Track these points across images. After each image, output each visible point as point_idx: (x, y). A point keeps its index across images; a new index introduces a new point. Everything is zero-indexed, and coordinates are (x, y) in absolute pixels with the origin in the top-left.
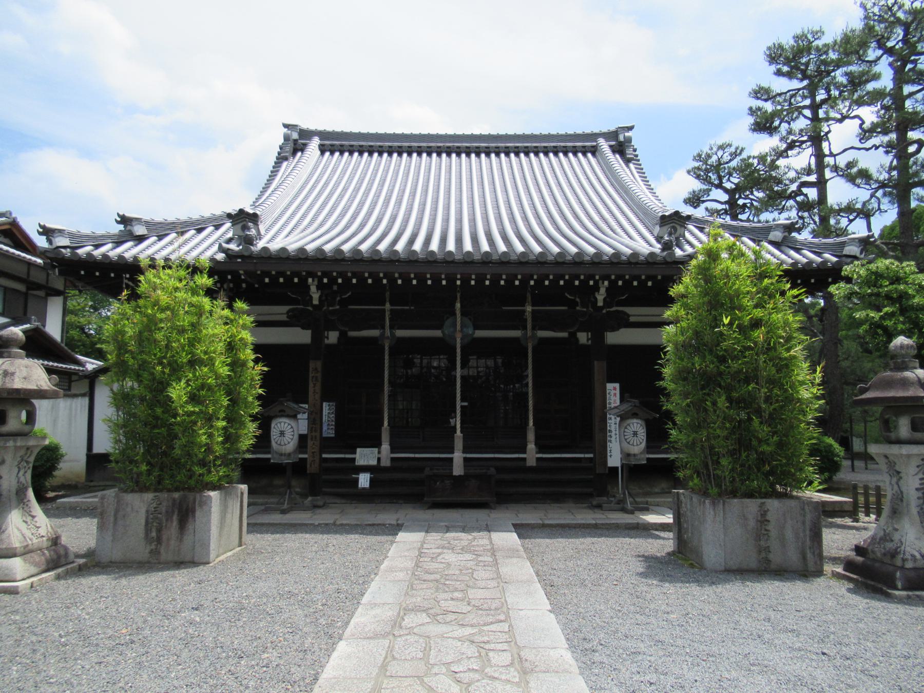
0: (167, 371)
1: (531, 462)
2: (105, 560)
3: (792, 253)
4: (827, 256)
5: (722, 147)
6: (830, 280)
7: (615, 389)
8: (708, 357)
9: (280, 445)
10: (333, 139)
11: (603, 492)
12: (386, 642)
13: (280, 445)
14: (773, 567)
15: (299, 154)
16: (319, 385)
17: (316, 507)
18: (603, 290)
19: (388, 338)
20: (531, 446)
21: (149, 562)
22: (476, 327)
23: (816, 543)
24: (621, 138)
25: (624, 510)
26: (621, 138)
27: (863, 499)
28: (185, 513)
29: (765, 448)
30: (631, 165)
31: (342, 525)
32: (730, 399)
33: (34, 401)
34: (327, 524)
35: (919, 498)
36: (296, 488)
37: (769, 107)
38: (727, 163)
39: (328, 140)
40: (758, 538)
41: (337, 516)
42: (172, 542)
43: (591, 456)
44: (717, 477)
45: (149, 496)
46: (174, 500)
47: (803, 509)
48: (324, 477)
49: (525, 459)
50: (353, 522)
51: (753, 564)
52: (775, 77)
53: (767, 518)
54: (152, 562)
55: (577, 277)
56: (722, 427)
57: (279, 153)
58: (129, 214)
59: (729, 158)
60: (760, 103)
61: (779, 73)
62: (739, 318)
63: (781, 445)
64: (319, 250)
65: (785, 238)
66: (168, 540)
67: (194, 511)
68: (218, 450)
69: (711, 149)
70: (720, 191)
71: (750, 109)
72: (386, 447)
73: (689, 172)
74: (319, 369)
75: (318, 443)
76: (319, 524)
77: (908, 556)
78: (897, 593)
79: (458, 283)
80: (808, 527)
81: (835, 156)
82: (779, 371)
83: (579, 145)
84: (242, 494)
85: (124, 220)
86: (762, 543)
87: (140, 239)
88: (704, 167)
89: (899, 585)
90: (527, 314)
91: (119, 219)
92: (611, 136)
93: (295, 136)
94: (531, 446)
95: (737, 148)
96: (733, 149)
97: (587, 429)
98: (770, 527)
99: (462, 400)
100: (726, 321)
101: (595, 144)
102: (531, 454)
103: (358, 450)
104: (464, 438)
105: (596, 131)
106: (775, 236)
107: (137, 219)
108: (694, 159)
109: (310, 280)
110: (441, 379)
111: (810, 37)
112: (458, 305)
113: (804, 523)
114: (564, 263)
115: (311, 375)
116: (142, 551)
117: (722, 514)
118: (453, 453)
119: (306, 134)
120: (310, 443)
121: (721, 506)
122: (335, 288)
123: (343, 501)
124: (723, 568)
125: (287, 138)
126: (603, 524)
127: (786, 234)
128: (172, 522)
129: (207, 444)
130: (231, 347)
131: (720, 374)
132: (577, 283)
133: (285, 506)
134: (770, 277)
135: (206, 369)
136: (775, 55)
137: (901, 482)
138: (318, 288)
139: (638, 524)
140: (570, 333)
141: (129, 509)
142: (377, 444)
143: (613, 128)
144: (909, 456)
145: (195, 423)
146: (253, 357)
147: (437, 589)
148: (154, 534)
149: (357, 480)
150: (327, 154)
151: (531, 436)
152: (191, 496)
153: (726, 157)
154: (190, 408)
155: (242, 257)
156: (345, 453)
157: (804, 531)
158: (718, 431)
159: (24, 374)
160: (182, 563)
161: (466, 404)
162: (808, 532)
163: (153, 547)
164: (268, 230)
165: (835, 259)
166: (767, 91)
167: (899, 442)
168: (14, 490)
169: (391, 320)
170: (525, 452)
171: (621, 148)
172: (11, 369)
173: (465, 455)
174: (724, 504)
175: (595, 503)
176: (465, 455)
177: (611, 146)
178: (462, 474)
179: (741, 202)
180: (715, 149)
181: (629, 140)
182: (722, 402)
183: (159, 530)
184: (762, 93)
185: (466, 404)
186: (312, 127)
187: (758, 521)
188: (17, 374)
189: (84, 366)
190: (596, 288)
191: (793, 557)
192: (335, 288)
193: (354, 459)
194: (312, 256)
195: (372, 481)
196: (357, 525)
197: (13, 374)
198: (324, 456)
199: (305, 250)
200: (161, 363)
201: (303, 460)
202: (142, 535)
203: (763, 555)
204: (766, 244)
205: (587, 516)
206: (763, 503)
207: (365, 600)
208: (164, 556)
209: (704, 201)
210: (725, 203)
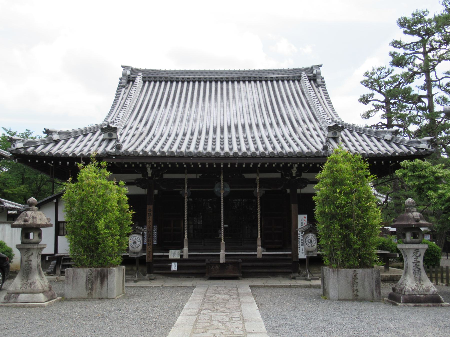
0: (95, 215)
2: (69, 297)
3: (394, 145)
4: (412, 148)
5: (379, 69)
7: (305, 218)
8: (332, 206)
9: (134, 248)
10: (150, 74)
11: (296, 271)
12: (196, 316)
13: (134, 248)
14: (359, 298)
15: (131, 83)
17: (151, 279)
18: (295, 169)
19: (187, 193)
20: (259, 248)
21: (88, 298)
24: (315, 72)
25: (306, 280)
26: (315, 72)
28: (103, 277)
29: (356, 246)
30: (320, 88)
31: (166, 287)
32: (342, 226)
33: (41, 228)
34: (158, 286)
36: (146, 267)
37: (401, 52)
38: (384, 78)
39: (148, 75)
40: (353, 285)
41: (163, 283)
43: (291, 253)
44: (336, 260)
45: (87, 269)
46: (98, 271)
47: (373, 273)
48: (154, 265)
49: (256, 255)
50: (172, 285)
51: (351, 297)
52: (404, 34)
53: (357, 277)
54: (90, 297)
56: (338, 237)
57: (120, 83)
58: (51, 128)
59: (385, 75)
60: (396, 50)
61: (405, 32)
62: (345, 189)
63: (364, 245)
65: (393, 138)
66: (96, 288)
67: (107, 276)
68: (116, 249)
69: (374, 70)
70: (380, 95)
71: (390, 53)
72: (186, 249)
73: (362, 83)
74: (152, 209)
75: (151, 247)
76: (155, 286)
77: (407, 290)
78: (400, 304)
79: (222, 166)
80: (374, 281)
81: (439, 80)
82: (363, 212)
83: (290, 77)
84: (124, 269)
85: (48, 132)
87: (57, 142)
88: (370, 81)
89: (402, 301)
90: (257, 180)
91: (45, 131)
92: (311, 69)
93: (129, 73)
94: (259, 248)
95: (389, 70)
96: (387, 70)
97: (287, 239)
98: (358, 281)
99: (225, 224)
100: (338, 191)
101: (299, 75)
102: (260, 252)
103: (170, 251)
104: (225, 244)
105: (301, 67)
106: (388, 137)
107: (55, 131)
108: (364, 75)
109: (148, 165)
111: (422, 14)
113: (373, 279)
114: (274, 157)
115: (147, 213)
116: (84, 293)
118: (220, 252)
119: (135, 71)
120: (148, 247)
121: (337, 272)
125: (124, 75)
126: (294, 286)
127: (394, 136)
128: (97, 280)
129: (112, 246)
130: (119, 202)
131: (338, 214)
133: (136, 279)
134: (362, 169)
135: (112, 214)
136: (403, 23)
137: (408, 260)
138: (151, 169)
139: (311, 285)
140: (300, 175)
141: (79, 275)
142: (181, 247)
143: (310, 66)
144: (409, 249)
145: (107, 237)
146: (129, 207)
147: (214, 305)
148: (90, 286)
150: (147, 83)
151: (259, 243)
152: (105, 269)
153: (383, 74)
154: (106, 231)
155: (116, 155)
156: (164, 253)
157: (373, 282)
158: (336, 239)
159: (40, 218)
160: (102, 298)
161: (227, 226)
162: (374, 283)
163: (90, 292)
164: (121, 134)
165: (415, 150)
166: (399, 43)
167: (407, 243)
168: (36, 266)
169: (188, 184)
170: (256, 251)
171: (314, 77)
172: (35, 216)
173: (226, 253)
174: (338, 271)
175: (292, 276)
176: (226, 253)
177: (308, 77)
178: (225, 262)
179: (392, 101)
180: (376, 70)
181: (319, 74)
182: (337, 226)
183: (92, 284)
184: (397, 44)
185: (227, 226)
186: (138, 67)
188: (38, 218)
189: (3, 204)
190: (292, 167)
193: (168, 256)
195: (178, 267)
196: (174, 287)
197: (36, 218)
198: (154, 254)
200: (92, 211)
201: (145, 256)
202: (85, 286)
203: (355, 293)
204: (382, 141)
205: (287, 282)
207: (185, 307)
208: (94, 296)
209: (370, 101)
210: (383, 102)
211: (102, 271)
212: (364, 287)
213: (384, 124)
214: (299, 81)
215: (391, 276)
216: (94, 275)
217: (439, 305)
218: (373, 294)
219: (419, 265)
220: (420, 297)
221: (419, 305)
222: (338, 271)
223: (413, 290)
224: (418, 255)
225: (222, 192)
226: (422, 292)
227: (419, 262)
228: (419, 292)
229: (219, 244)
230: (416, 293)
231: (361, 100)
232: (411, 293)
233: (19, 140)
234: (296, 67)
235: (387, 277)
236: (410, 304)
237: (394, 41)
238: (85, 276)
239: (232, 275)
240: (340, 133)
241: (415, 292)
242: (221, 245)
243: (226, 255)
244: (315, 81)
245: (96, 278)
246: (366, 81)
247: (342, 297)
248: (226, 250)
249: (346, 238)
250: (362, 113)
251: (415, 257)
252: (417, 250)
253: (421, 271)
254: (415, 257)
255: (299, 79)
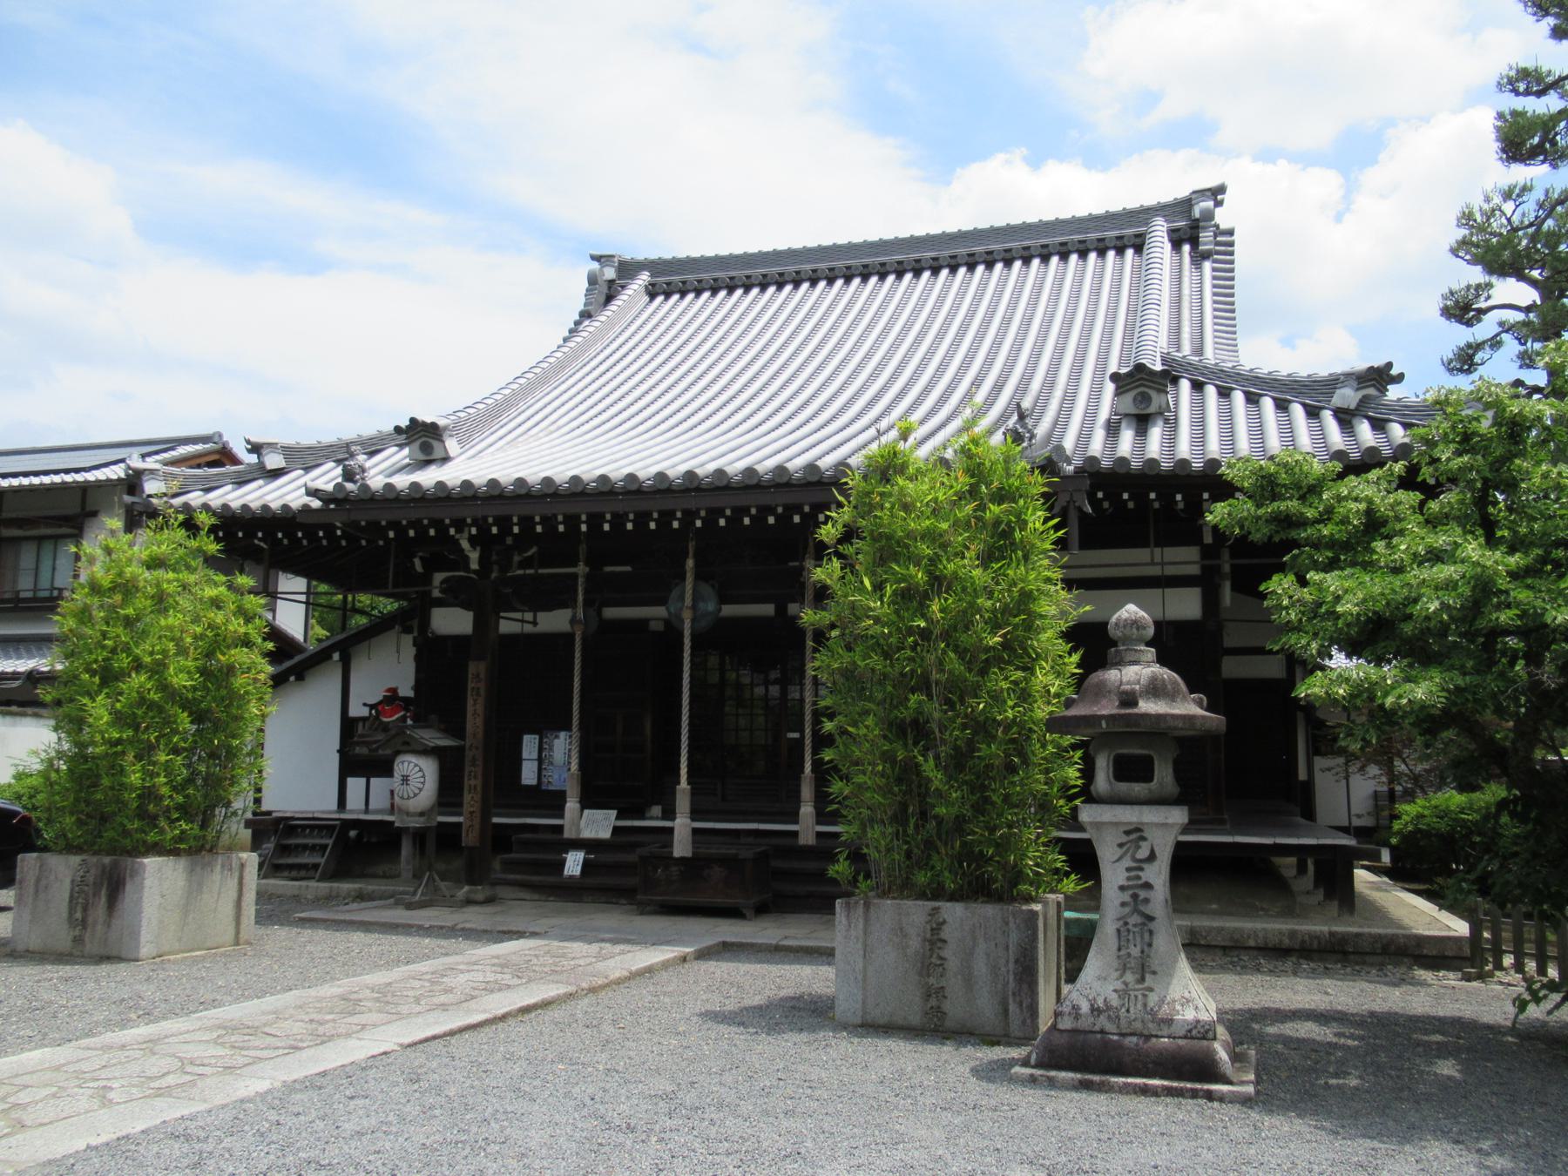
1: (807, 838)
2: (20, 947)
6: (1206, 496)
10: (671, 273)
14: (948, 1024)
16: (481, 701)
21: (71, 955)
22: (724, 599)
23: (1025, 986)
24: (1197, 213)
27: (1504, 934)
28: (113, 886)
30: (1207, 265)
35: (1123, 904)
42: (99, 927)
45: (75, 860)
46: (104, 866)
47: (1007, 924)
49: (795, 834)
51: (915, 1019)
53: (943, 935)
55: (770, 510)
64: (780, 469)
65: (1364, 401)
69: (1488, 200)
74: (482, 676)
79: (584, 528)
80: (1012, 960)
86: (932, 980)
93: (610, 273)
98: (946, 953)
105: (1150, 201)
106: (1343, 397)
107: (270, 445)
110: (589, 690)
112: (690, 563)
115: (470, 685)
116: (63, 937)
117: (861, 926)
118: (673, 819)
119: (628, 269)
121: (860, 910)
122: (509, 541)
123: (536, 897)
124: (859, 1022)
125: (593, 280)
127: (1372, 391)
132: (771, 520)
143: (1183, 192)
148: (79, 915)
149: (563, 863)
162: (1011, 966)
163: (77, 933)
169: (586, 592)
170: (797, 822)
171: (1193, 228)
174: (867, 906)
183: (85, 910)
184: (1530, 81)
187: (925, 940)
191: (985, 1006)
192: (509, 541)
193: (560, 828)
194: (769, 481)
195: (586, 865)
199: (817, 467)
202: (65, 915)
206: (936, 909)
208: (91, 947)
210: (1528, 309)
211: (115, 865)
212: (969, 981)
213: (1536, 389)
214: (1139, 249)
215: (1332, 934)
216: (91, 879)
217: (1194, 1094)
218: (1006, 1011)
219: (1147, 901)
220: (1119, 1046)
221: (1102, 1083)
222: (867, 906)
223: (1095, 1011)
224: (1143, 853)
225: (687, 616)
226: (1138, 1026)
227: (1148, 886)
228: (1123, 1022)
229: (796, 800)
230: (1110, 1027)
231: (1447, 313)
232: (1085, 1023)
233: (152, 471)
234: (1133, 204)
235: (1317, 937)
236: (1063, 1075)
237: (1512, 73)
238: (67, 882)
239: (720, 901)
240: (1162, 396)
241: (1103, 1022)
242: (678, 796)
243: (695, 831)
244: (1194, 242)
245: (97, 886)
246: (1464, 243)
247: (878, 1014)
248: (696, 814)
249: (907, 774)
250: (1449, 354)
251: (1127, 862)
252: (1136, 833)
253: (1152, 926)
254: (1127, 862)
255: (1138, 241)
